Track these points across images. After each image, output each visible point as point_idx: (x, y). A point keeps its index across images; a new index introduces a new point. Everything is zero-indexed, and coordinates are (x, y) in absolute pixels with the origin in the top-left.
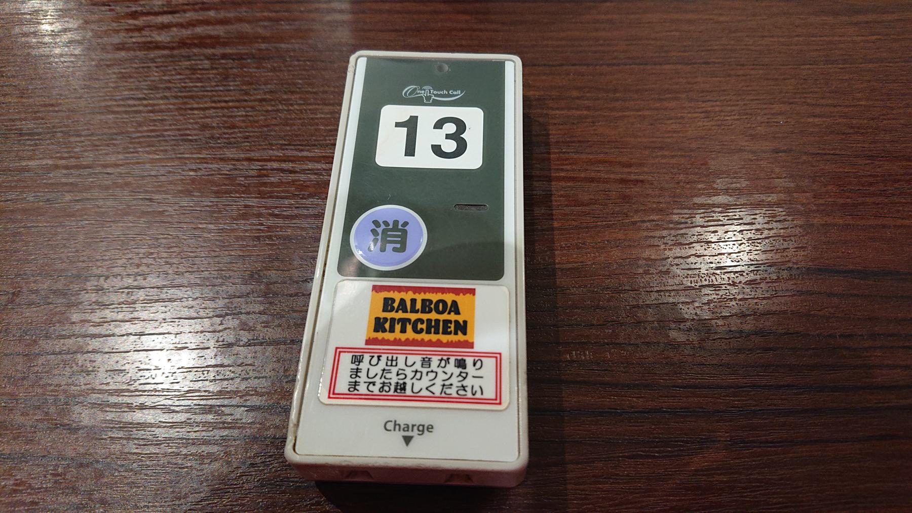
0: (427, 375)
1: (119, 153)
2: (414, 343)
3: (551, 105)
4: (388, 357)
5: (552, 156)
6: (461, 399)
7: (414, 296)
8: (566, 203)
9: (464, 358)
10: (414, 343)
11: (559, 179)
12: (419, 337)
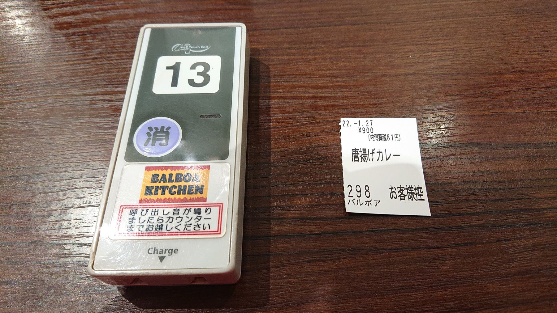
0: (176, 219)
1: (9, 96)
2: (169, 200)
3: (272, 53)
4: (152, 210)
5: (271, 84)
6: (196, 233)
7: (171, 172)
8: (279, 112)
9: (200, 208)
10: (169, 200)
11: (275, 98)
12: (172, 197)
